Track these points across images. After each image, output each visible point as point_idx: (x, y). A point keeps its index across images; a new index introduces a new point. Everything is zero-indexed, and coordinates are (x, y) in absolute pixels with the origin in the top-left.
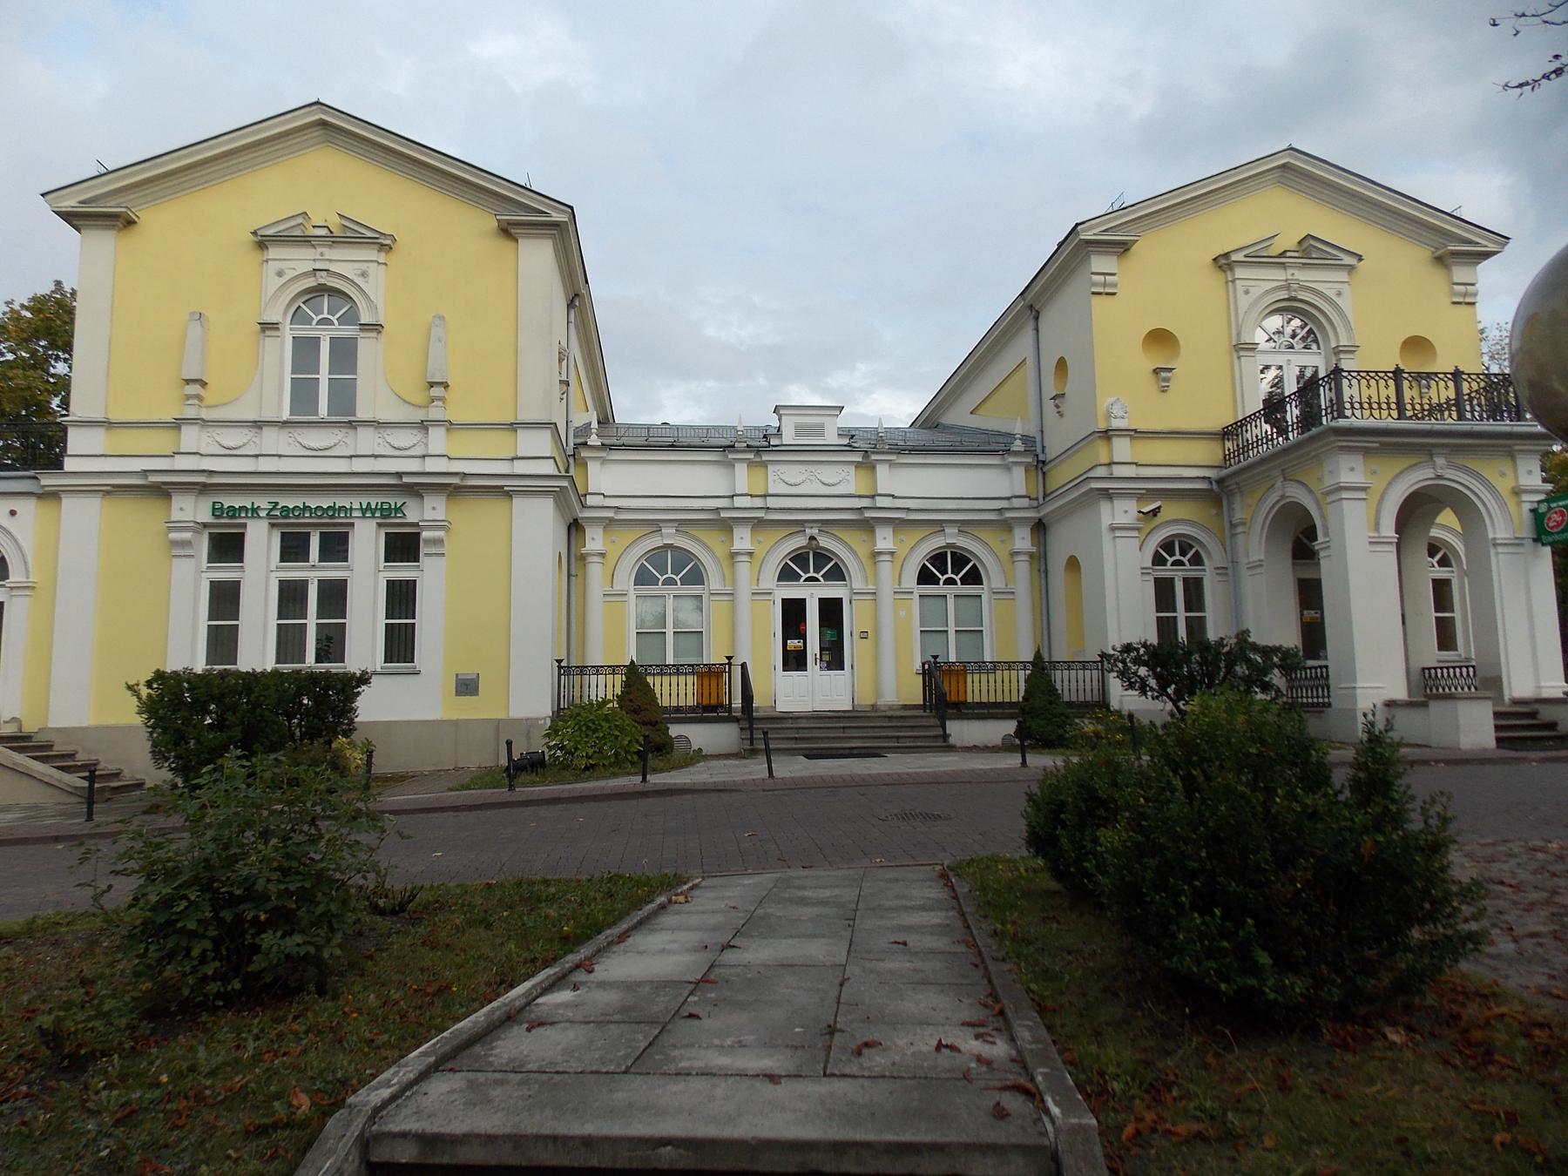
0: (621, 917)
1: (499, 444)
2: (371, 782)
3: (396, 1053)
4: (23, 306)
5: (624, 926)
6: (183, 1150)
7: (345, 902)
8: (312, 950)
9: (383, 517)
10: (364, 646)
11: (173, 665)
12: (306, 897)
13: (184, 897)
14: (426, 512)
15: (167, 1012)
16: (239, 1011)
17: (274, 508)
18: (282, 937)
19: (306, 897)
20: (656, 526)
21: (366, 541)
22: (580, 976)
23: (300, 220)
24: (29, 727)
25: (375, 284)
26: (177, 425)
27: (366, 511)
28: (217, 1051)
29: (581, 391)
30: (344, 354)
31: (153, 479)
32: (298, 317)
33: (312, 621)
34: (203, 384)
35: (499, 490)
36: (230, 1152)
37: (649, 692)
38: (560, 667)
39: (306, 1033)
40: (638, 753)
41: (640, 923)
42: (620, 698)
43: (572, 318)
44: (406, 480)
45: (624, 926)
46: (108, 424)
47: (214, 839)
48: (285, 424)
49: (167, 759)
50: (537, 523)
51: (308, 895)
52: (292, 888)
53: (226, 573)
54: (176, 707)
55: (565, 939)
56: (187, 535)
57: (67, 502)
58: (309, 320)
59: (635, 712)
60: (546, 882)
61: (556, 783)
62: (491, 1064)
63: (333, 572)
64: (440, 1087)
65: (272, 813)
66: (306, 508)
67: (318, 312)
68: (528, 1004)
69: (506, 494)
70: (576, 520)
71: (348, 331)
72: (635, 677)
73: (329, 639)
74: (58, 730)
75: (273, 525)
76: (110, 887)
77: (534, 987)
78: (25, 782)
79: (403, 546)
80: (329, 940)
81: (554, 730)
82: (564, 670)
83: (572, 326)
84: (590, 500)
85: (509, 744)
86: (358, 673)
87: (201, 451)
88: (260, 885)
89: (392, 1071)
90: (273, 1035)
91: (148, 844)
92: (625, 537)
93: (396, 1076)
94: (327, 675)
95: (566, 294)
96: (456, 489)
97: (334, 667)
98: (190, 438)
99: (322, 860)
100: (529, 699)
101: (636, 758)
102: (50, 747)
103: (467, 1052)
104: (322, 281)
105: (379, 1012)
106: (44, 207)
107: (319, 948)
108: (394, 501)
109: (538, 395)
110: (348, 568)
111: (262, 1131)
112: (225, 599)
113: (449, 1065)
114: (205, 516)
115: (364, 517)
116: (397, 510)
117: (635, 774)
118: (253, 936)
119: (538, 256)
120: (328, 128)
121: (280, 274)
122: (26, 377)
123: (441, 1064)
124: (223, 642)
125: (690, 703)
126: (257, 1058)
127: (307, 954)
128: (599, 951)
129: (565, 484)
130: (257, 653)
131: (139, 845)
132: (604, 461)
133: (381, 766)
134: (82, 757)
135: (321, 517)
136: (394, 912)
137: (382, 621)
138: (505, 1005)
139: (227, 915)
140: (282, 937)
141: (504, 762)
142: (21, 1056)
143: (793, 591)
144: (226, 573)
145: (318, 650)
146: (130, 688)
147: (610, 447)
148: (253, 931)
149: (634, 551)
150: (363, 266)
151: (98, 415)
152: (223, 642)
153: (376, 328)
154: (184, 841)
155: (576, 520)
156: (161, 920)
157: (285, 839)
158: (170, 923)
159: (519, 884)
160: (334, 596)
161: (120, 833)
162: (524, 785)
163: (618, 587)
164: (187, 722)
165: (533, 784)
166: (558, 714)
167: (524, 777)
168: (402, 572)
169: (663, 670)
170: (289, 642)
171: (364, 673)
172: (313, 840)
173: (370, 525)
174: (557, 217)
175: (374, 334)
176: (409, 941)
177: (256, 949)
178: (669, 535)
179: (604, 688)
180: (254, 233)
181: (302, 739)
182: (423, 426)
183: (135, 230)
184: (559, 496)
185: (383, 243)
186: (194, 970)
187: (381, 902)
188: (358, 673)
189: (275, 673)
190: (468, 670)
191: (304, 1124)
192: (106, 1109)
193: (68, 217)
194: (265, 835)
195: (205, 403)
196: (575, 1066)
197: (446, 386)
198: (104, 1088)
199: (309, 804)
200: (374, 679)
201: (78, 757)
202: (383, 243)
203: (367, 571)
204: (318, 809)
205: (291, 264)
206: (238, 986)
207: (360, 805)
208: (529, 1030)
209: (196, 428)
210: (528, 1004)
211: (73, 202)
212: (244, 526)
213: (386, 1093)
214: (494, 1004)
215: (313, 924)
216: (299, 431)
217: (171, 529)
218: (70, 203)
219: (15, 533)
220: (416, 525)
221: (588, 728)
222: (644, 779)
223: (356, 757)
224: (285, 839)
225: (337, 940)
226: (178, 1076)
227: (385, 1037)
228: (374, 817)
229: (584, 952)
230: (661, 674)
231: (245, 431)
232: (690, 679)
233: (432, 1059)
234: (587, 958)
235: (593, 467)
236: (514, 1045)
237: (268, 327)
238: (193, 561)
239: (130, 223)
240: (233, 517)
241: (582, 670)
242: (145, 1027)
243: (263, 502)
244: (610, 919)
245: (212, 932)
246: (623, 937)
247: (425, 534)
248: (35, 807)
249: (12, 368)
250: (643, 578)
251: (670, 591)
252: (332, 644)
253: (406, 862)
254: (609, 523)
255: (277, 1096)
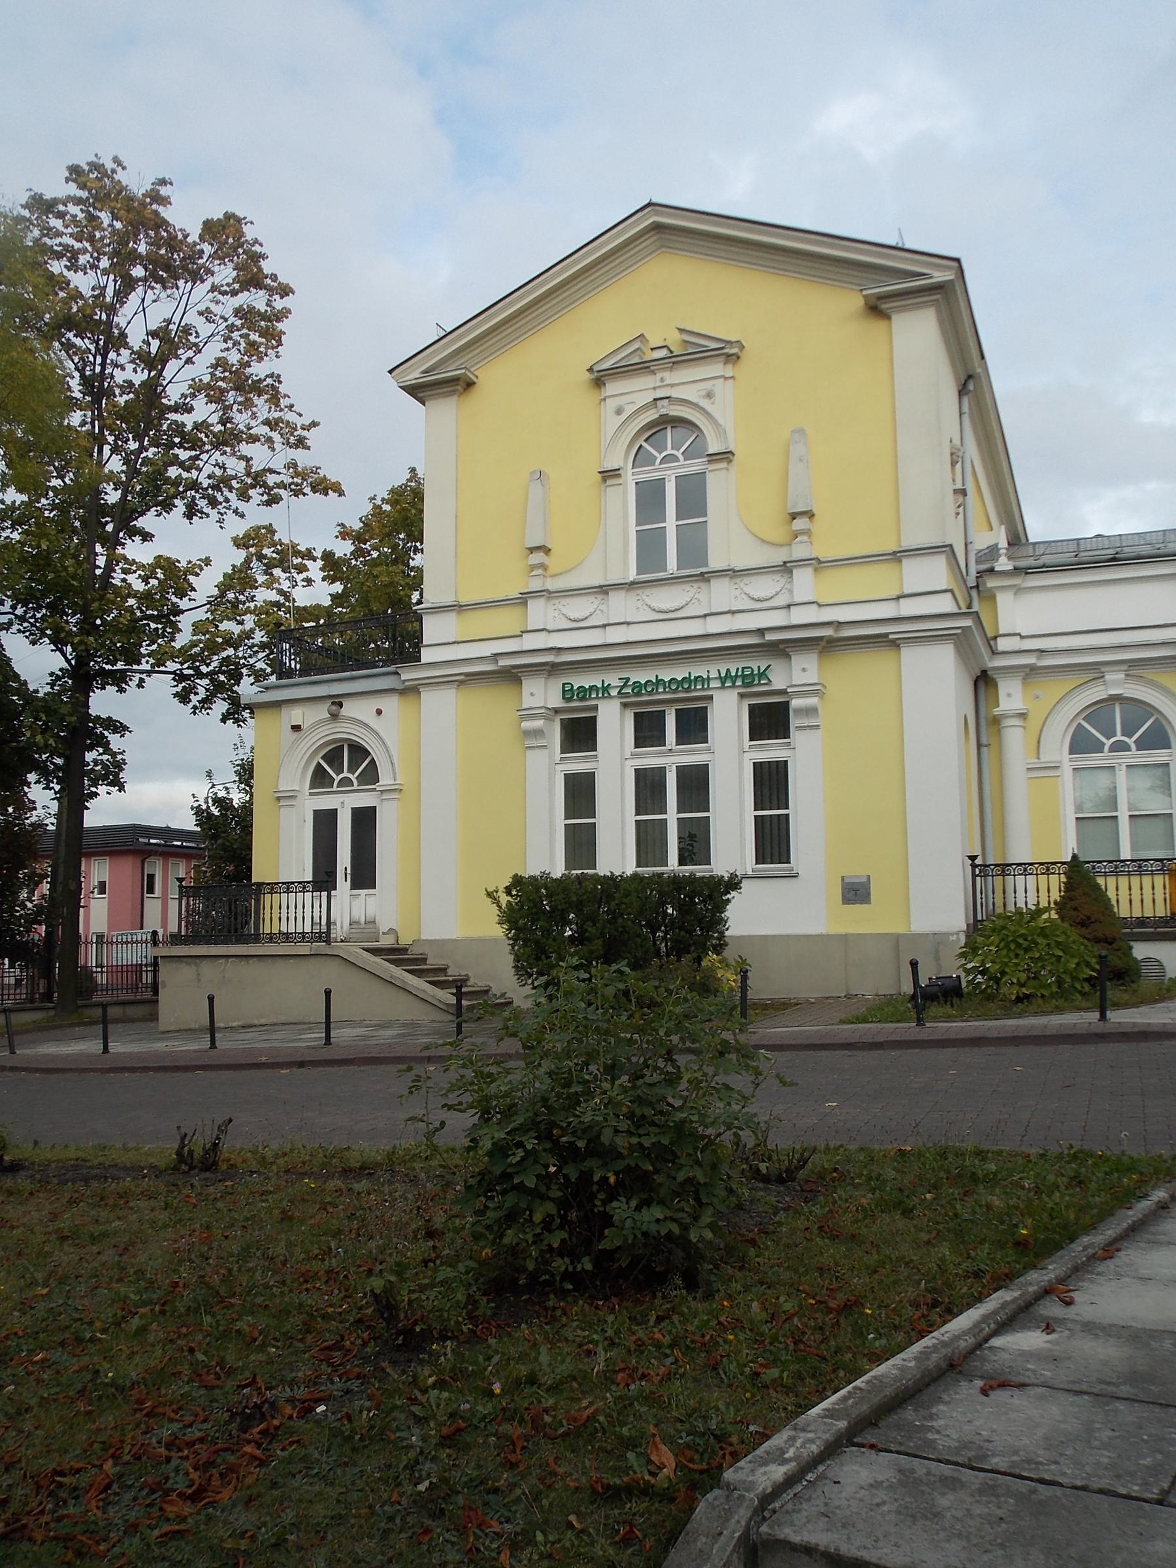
0: (1104, 1215)
1: (878, 581)
2: (745, 1007)
3: (789, 1401)
4: (383, 499)
5: (1109, 1232)
6: (518, 1500)
7: (714, 1166)
8: (676, 1230)
9: (745, 685)
10: (732, 846)
11: (532, 870)
12: (664, 1155)
13: (520, 1145)
14: (795, 675)
15: (512, 1289)
16: (593, 1298)
17: (625, 685)
18: (638, 1209)
19: (664, 1155)
20: (1096, 671)
21: (728, 715)
22: (1051, 1309)
23: (636, 345)
24: (405, 940)
25: (721, 403)
26: (523, 600)
27: (726, 680)
28: (566, 1352)
29: (981, 503)
30: (693, 498)
31: (503, 662)
32: (640, 458)
33: (672, 816)
34: (546, 550)
35: (882, 641)
36: (572, 1518)
37: (1099, 895)
38: (974, 866)
39: (671, 1346)
40: (1089, 980)
41: (1134, 1229)
42: (1060, 906)
43: (966, 408)
44: (769, 637)
45: (1109, 1232)
46: (458, 608)
47: (550, 1074)
48: (632, 585)
49: (530, 975)
50: (933, 680)
51: (665, 1158)
52: (647, 1143)
53: (579, 764)
54: (537, 914)
55: (1021, 1245)
56: (539, 723)
57: (426, 696)
58: (651, 460)
59: (1082, 924)
60: (980, 1154)
61: (978, 1018)
62: (931, 1444)
63: (692, 756)
64: (859, 1473)
65: (619, 1040)
66: (659, 682)
67: (661, 448)
68: (979, 1346)
69: (890, 643)
70: (984, 672)
71: (694, 466)
72: (1078, 876)
73: (692, 837)
74: (431, 942)
75: (625, 705)
76: (443, 1124)
77: (985, 1319)
78: (403, 997)
79: (770, 720)
80: (696, 1219)
81: (971, 948)
82: (979, 869)
83: (966, 417)
84: (1003, 644)
85: (914, 964)
86: (726, 876)
87: (551, 627)
88: (606, 1137)
89: (786, 1434)
90: (630, 1343)
91: (480, 1074)
92: (1054, 689)
93: (795, 1442)
94: (692, 879)
95: (957, 378)
96: (829, 643)
97: (699, 870)
98: (538, 614)
99: (681, 1108)
100: (937, 908)
101: (1087, 987)
102: (424, 960)
103: (894, 1418)
104: (663, 411)
105: (765, 1328)
106: (391, 384)
107: (685, 1228)
108: (756, 664)
109: (928, 513)
110: (708, 751)
111: (612, 1495)
112: (580, 793)
113: (870, 1437)
114: (556, 701)
115: (723, 687)
116: (762, 675)
117: (1087, 1009)
118: (605, 1203)
119: (918, 333)
120: (666, 231)
121: (619, 412)
122: (389, 574)
123: (854, 1436)
124: (581, 843)
125: (1161, 912)
126: (608, 1377)
127: (669, 1234)
128: (1076, 1269)
129: (967, 622)
130: (617, 856)
131: (469, 1074)
132: (1018, 591)
133: (759, 990)
134: (453, 972)
135: (675, 691)
136: (781, 1181)
137: (750, 813)
138: (944, 1344)
139: (572, 1172)
140: (638, 1209)
141: (908, 988)
142: (359, 1321)
143: (326, 802)
144: (579, 764)
145: (680, 850)
146: (489, 895)
147: (1026, 571)
148: (602, 1196)
149: (1067, 707)
150: (708, 385)
151: (449, 600)
152: (581, 843)
153: (726, 456)
154: (518, 1073)
155: (984, 672)
156: (497, 1170)
157: (637, 1077)
158: (506, 1176)
159: (943, 1155)
160: (695, 784)
161: (450, 1057)
162: (935, 1019)
163: (1048, 757)
164: (547, 932)
165: (948, 1018)
166: (975, 927)
167: (935, 1010)
168: (770, 751)
169: (1118, 867)
170: (649, 841)
171: (733, 876)
172: (672, 1080)
173: (733, 695)
174: (939, 276)
175: (724, 465)
176: (801, 1223)
177: (607, 1220)
178: (1115, 683)
179: (1037, 893)
180: (591, 370)
181: (668, 955)
182: (786, 568)
183: (476, 388)
184: (962, 641)
185: (727, 353)
186: (538, 1238)
187: (763, 1167)
188: (726, 876)
189: (635, 876)
190: (856, 871)
191: (667, 1496)
192: (434, 1417)
193: (414, 390)
194: (612, 1070)
195: (550, 572)
196: (1068, 1473)
197: (810, 515)
198: (434, 1386)
199: (662, 1033)
200: (745, 884)
201: (450, 971)
202: (727, 353)
203: (729, 753)
204: (675, 1038)
205: (629, 398)
206: (589, 1267)
207: (727, 1035)
208: (984, 1392)
209: (542, 601)
210: (979, 1346)
211: (416, 374)
212: (595, 708)
213: (778, 1472)
214: (927, 1341)
215: (676, 1194)
216: (648, 592)
217: (523, 718)
218: (413, 375)
219: (382, 734)
220: (783, 692)
221: (1019, 945)
222: (1103, 1017)
223: (730, 978)
224: (637, 1077)
225: (707, 1218)
226: (515, 1386)
227: (774, 1372)
228: (746, 1054)
229: (1052, 1270)
230: (1116, 873)
231: (591, 598)
232: (1159, 880)
233: (842, 1424)
234: (1061, 1281)
235: (1004, 601)
236: (961, 1416)
237: (609, 475)
238: (545, 752)
239: (470, 384)
240: (583, 699)
241: (1004, 869)
242: (485, 1307)
243: (613, 679)
244: (1087, 1220)
245: (555, 1193)
246: (1109, 1251)
247: (795, 703)
248: (412, 1025)
249: (377, 566)
250: (1080, 744)
251: (1121, 760)
252: (695, 843)
253: (792, 1114)
254: (1030, 673)
255: (631, 1444)
